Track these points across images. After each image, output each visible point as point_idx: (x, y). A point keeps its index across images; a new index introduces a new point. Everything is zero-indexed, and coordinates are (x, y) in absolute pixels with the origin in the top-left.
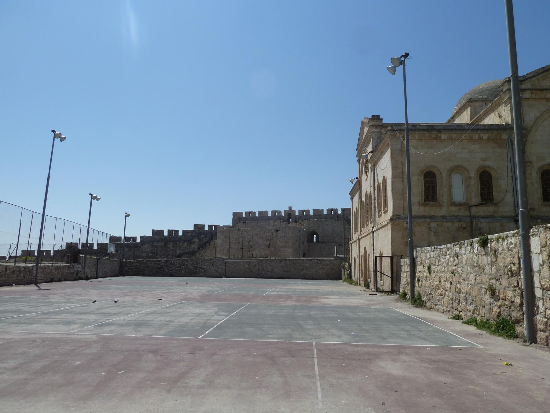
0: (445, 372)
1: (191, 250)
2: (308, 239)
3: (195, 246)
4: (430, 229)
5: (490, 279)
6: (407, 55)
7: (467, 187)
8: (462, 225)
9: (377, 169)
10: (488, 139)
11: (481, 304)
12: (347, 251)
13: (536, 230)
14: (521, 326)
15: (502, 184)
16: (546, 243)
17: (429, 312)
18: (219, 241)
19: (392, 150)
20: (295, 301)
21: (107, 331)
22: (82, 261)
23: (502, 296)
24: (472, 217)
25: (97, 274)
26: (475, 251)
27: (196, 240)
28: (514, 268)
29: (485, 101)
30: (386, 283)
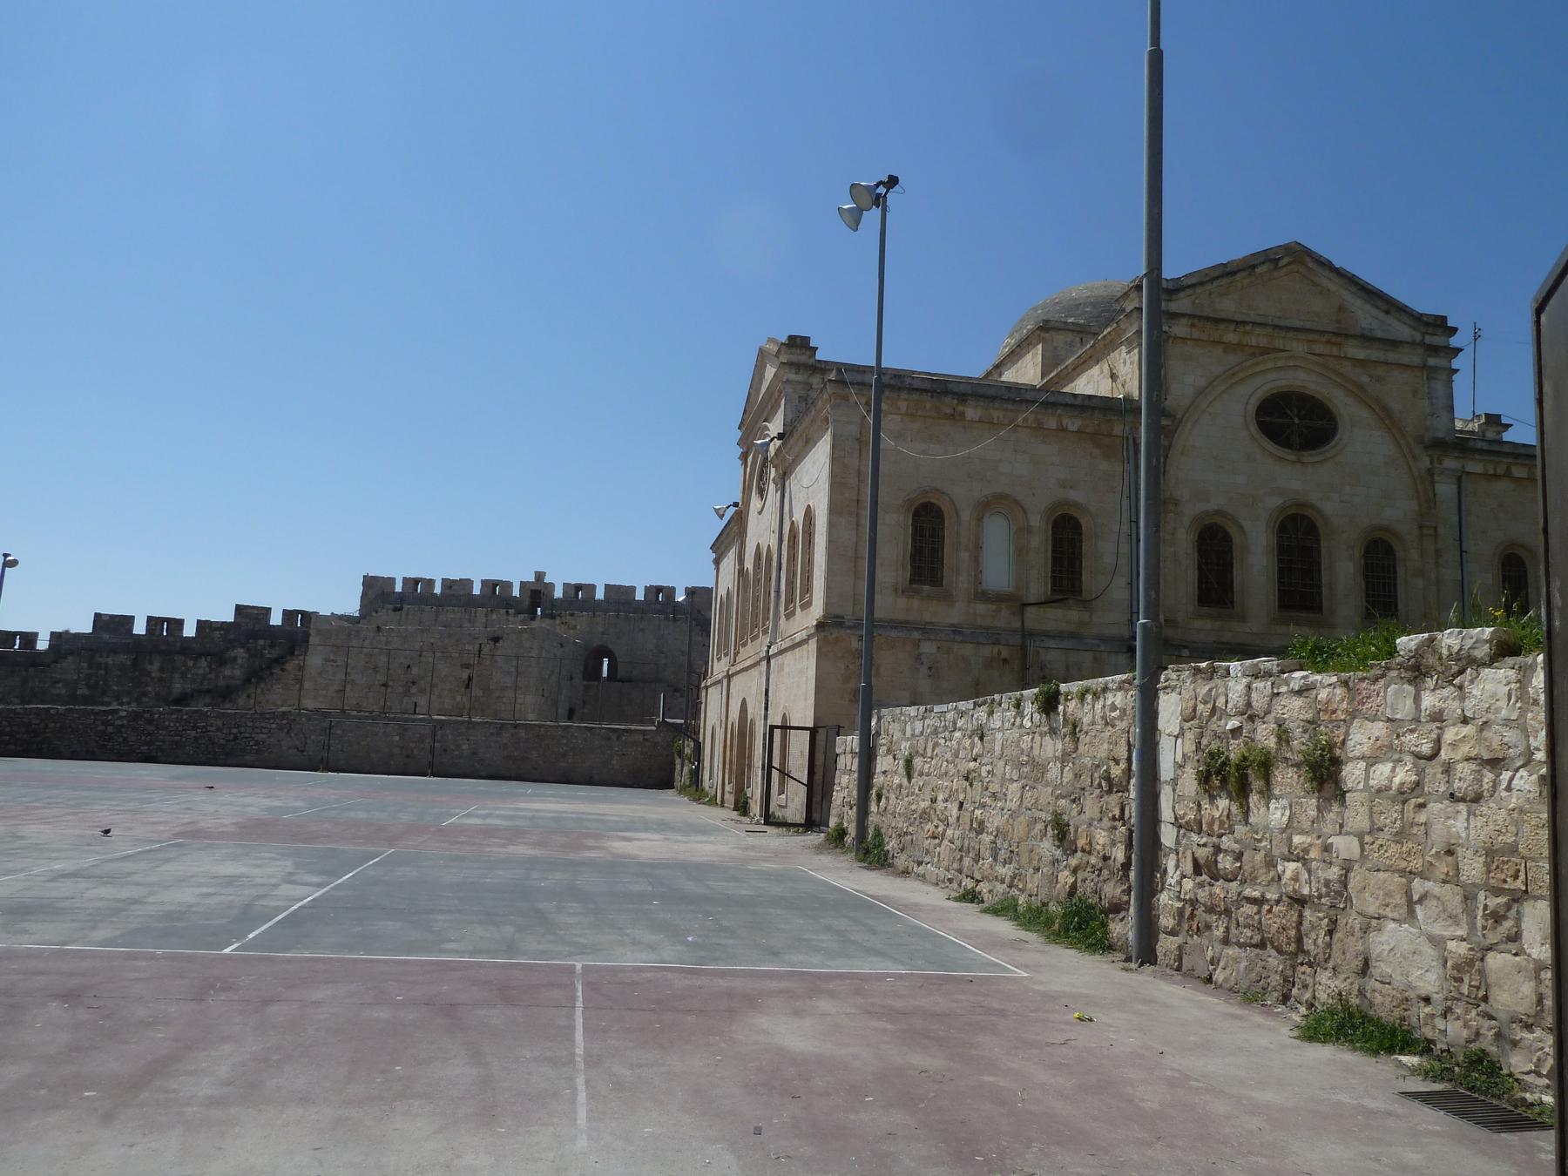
1: (222, 683)
2: (586, 667)
3: (234, 673)
4: (918, 658)
6: (892, 181)
7: (1020, 553)
8: (999, 653)
9: (793, 484)
10: (1079, 432)
11: (1030, 861)
12: (694, 709)
15: (1104, 552)
18: (315, 660)
19: (834, 437)
20: (534, 845)
23: (1081, 842)
24: (1027, 634)
27: (240, 652)
28: (1116, 771)
29: (1082, 332)
30: (793, 802)
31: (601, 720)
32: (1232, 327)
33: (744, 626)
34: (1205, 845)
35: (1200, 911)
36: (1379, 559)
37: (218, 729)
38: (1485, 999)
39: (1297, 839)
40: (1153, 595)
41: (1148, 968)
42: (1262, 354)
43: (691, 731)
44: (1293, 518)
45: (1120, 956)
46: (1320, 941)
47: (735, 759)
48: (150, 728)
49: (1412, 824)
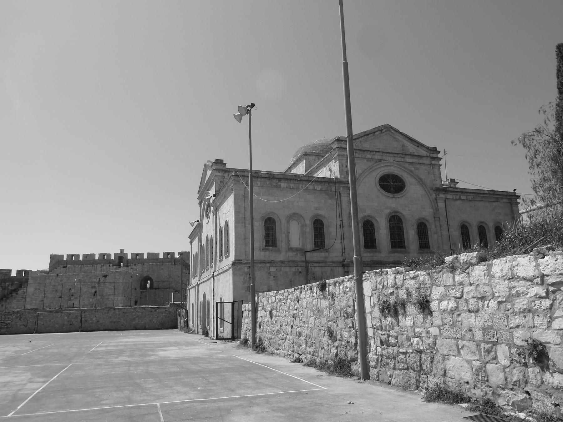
2: (141, 284)
5: (328, 322)
6: (253, 105)
7: (303, 233)
9: (220, 213)
10: (320, 190)
11: (320, 346)
13: (368, 275)
15: (332, 231)
16: (376, 287)
17: (270, 357)
18: (31, 289)
19: (235, 195)
20: (129, 356)
23: (338, 337)
24: (307, 262)
26: (315, 295)
28: (350, 310)
29: (318, 156)
30: (226, 330)
31: (148, 304)
32: (369, 152)
33: (203, 266)
35: (384, 358)
36: (422, 228)
38: (487, 381)
39: (417, 330)
42: (379, 161)
43: (184, 306)
45: (356, 378)
46: (428, 365)
49: (457, 321)
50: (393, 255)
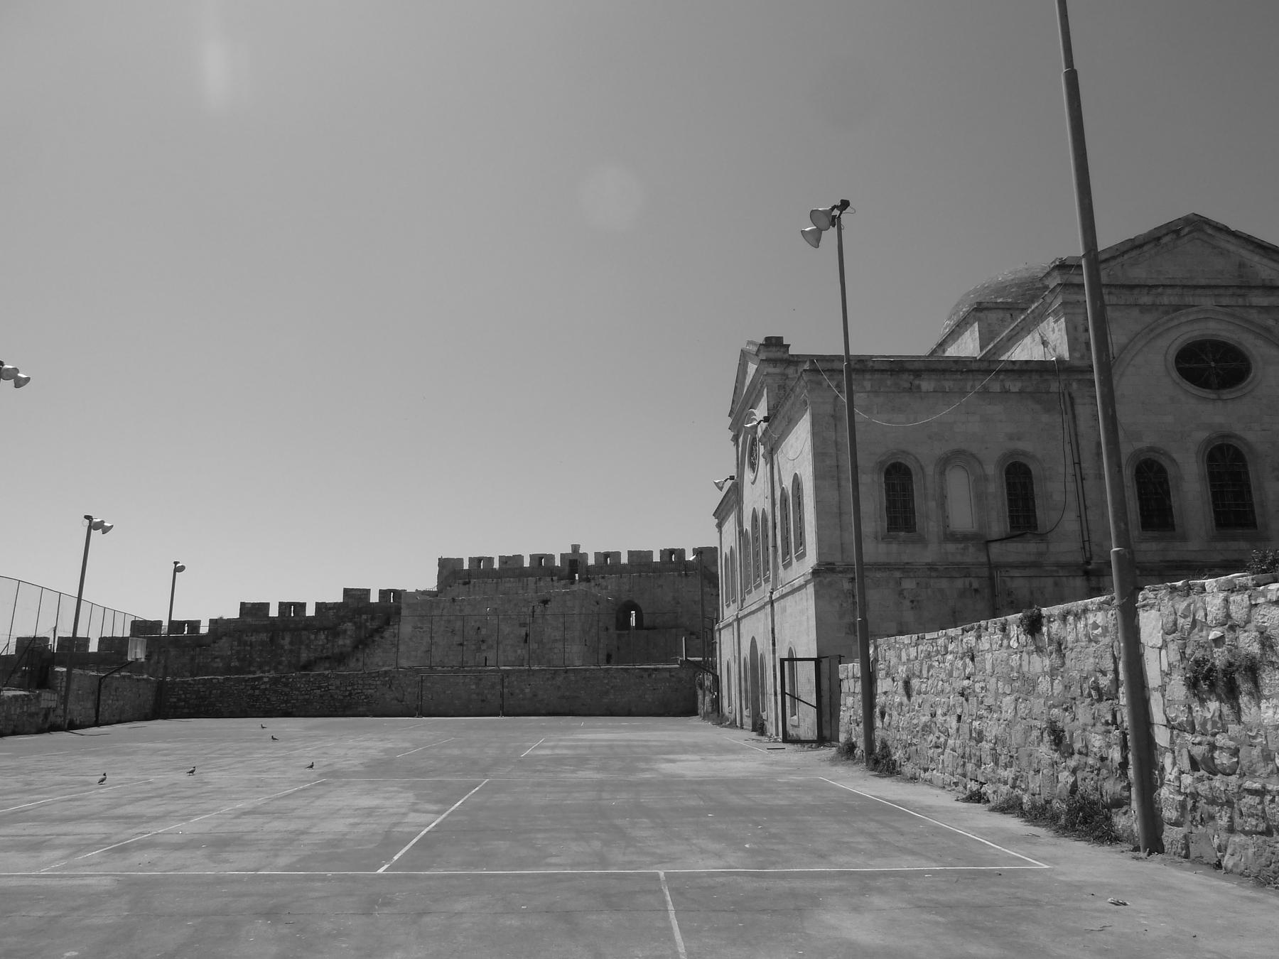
0: (977, 932)
1: (336, 651)
2: (618, 620)
3: (345, 642)
4: (901, 593)
6: (845, 205)
7: (980, 498)
8: (971, 585)
9: (780, 457)
10: (1021, 392)
12: (710, 648)
13: (1151, 595)
14: (1125, 813)
15: (1054, 490)
16: (1175, 623)
17: (910, 788)
18: (406, 628)
20: (598, 770)
21: (140, 864)
22: (61, 684)
23: (1078, 746)
24: (993, 567)
25: (97, 716)
26: (1014, 644)
27: (349, 626)
28: (1105, 682)
29: (1011, 309)
30: (805, 721)
31: (634, 662)
32: (1145, 291)
33: (748, 577)
34: (1200, 744)
37: (337, 688)
40: (1122, 525)
41: (1157, 857)
44: (1220, 448)
47: (749, 688)
48: (287, 690)
50: (1219, 545)
